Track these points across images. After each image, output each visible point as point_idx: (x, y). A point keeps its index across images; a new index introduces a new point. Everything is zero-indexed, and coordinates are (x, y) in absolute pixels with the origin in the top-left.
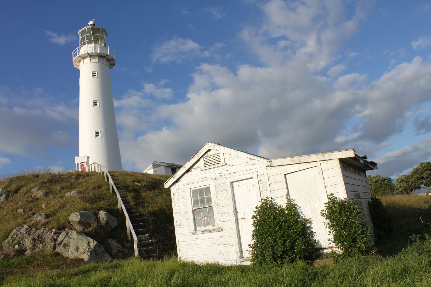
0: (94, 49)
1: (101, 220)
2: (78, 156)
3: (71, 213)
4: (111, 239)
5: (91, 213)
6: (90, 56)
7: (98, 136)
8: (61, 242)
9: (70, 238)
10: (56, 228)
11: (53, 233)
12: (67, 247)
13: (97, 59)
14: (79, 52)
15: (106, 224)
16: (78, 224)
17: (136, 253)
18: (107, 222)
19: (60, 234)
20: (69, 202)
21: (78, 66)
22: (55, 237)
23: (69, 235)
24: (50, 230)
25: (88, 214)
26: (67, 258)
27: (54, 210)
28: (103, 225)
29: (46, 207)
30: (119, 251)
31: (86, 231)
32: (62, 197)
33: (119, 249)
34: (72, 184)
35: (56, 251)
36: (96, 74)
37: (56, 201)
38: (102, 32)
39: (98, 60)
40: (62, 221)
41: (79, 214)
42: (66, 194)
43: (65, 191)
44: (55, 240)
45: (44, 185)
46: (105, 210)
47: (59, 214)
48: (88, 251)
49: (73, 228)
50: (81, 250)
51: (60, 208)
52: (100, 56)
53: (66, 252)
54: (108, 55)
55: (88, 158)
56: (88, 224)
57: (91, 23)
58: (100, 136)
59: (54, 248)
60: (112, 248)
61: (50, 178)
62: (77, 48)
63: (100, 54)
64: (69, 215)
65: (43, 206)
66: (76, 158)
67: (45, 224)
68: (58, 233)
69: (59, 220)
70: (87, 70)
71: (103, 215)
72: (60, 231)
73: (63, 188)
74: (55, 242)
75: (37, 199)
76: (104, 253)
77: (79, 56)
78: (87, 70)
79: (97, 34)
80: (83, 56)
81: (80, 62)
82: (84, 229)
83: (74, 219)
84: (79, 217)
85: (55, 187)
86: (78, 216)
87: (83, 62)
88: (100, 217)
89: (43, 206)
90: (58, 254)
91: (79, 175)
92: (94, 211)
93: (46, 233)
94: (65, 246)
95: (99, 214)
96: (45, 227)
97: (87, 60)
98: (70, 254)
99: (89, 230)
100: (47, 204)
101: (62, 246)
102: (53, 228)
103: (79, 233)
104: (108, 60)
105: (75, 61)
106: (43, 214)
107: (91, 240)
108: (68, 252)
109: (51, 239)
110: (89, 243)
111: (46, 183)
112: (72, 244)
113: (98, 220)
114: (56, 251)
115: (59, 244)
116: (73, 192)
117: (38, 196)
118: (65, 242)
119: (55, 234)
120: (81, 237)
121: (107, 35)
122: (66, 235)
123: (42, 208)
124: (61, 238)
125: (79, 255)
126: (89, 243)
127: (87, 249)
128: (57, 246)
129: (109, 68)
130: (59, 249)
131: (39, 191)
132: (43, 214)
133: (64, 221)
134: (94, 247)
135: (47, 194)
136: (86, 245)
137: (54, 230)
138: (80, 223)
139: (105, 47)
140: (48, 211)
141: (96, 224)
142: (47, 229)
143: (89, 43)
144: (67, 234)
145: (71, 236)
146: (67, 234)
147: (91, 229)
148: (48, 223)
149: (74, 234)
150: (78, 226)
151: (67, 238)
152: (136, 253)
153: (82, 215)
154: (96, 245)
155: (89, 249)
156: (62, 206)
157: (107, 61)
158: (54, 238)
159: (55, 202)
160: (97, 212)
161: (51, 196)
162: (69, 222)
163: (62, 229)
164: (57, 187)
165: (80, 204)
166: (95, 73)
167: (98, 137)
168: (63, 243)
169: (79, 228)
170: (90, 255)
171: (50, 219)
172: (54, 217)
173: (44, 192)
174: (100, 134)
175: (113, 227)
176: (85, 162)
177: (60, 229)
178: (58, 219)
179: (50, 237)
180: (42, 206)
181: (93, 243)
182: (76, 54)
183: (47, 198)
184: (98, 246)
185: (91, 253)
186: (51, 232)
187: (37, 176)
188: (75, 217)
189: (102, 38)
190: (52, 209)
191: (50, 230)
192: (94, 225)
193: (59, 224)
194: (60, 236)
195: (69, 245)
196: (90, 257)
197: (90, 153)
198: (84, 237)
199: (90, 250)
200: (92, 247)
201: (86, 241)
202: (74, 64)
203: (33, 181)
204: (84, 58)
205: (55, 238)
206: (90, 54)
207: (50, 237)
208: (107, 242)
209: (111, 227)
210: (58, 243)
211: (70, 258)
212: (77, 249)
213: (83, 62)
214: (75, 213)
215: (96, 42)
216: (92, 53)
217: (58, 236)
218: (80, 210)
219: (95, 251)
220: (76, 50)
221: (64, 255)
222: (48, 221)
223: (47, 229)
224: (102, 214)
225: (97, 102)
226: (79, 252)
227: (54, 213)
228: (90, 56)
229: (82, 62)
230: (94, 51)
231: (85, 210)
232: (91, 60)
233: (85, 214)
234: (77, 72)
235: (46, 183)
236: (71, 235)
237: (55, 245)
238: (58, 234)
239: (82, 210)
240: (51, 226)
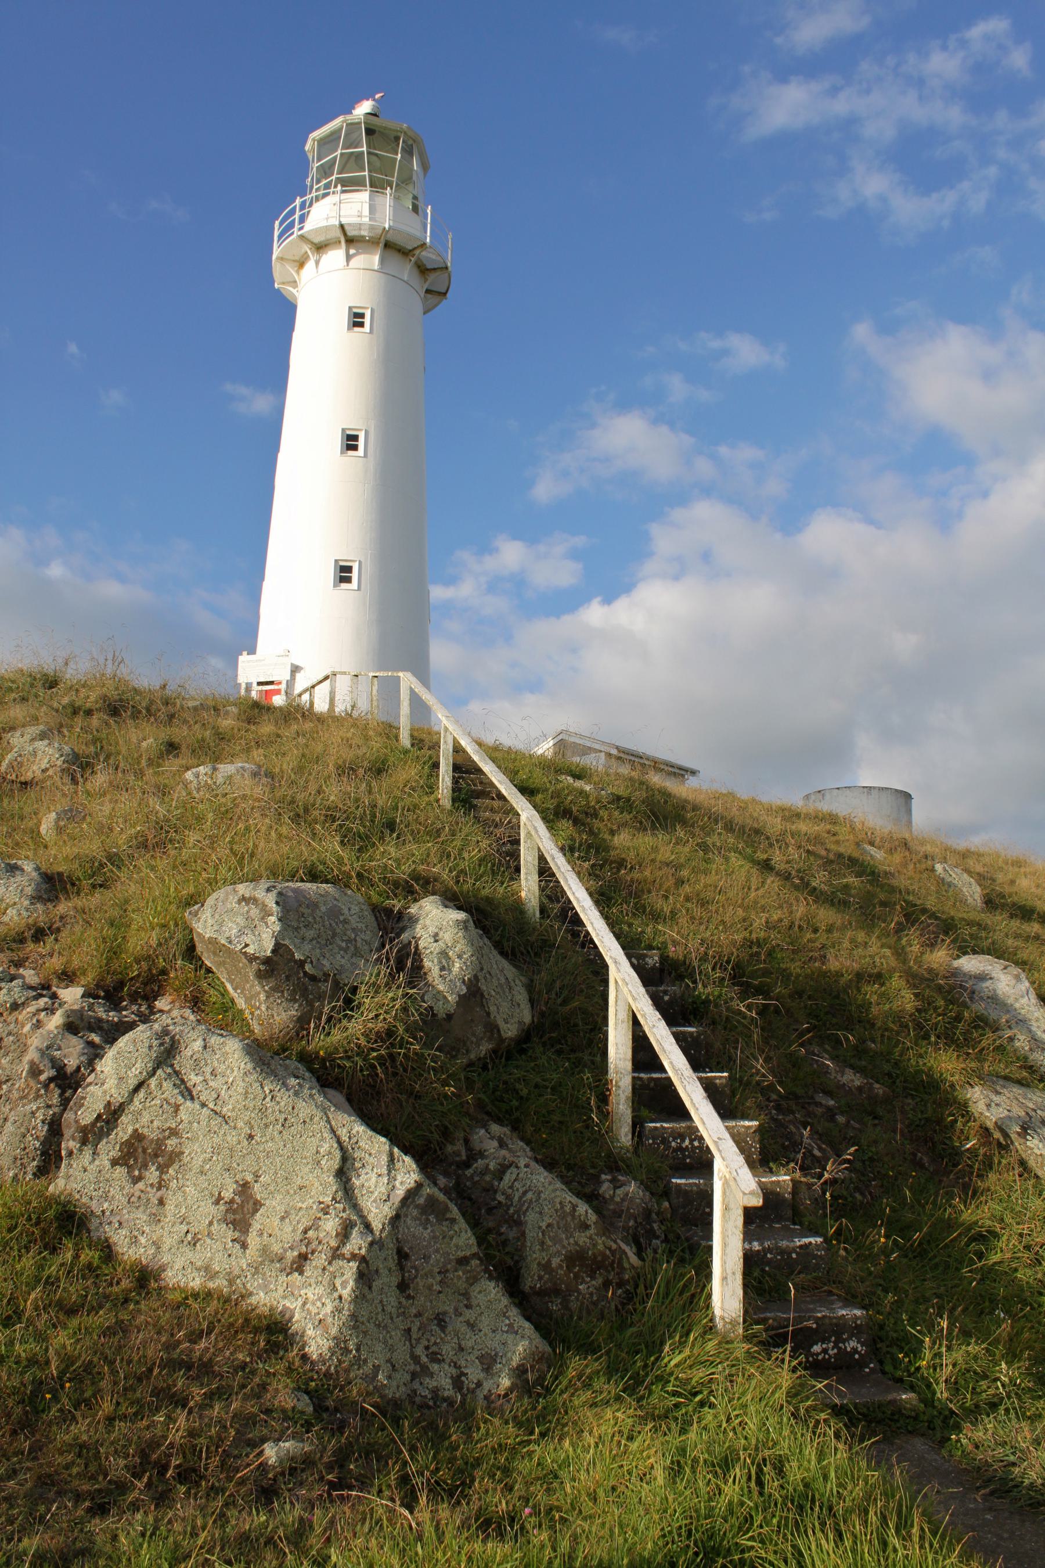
0: (366, 211)
1: (431, 964)
2: (252, 651)
3: (213, 884)
4: (495, 1128)
5: (353, 906)
6: (351, 240)
7: (348, 580)
8: (112, 1115)
9: (188, 1093)
10: (90, 977)
11: (56, 1021)
12: (152, 1174)
13: (376, 258)
14: (302, 219)
15: (463, 1000)
16: (260, 975)
17: (726, 1295)
18: (473, 994)
19: (113, 1033)
20: (200, 819)
21: (294, 283)
22: (72, 1054)
23: (183, 1061)
24: (44, 988)
25: (335, 913)
26: (145, 1278)
27: (101, 856)
28: (441, 1010)
29: (60, 830)
30: (577, 1258)
31: (319, 1042)
32: (163, 791)
33: (582, 1239)
34: (221, 737)
35: (59, 1185)
36: (367, 321)
37: (127, 803)
38: (408, 152)
39: (382, 261)
40: (142, 938)
41: (270, 901)
42: (189, 775)
43: (181, 761)
44: (67, 1082)
45: (79, 721)
46: (452, 899)
47: (127, 886)
48: (336, 1254)
49: (213, 995)
50: (275, 1226)
51: (144, 845)
52: (392, 247)
53: (141, 1216)
54: (423, 245)
55: (295, 669)
56: (337, 986)
57: (365, 107)
58: (354, 584)
59: (50, 1158)
60: (518, 1224)
61: (114, 694)
62: (298, 201)
63: (390, 237)
64: (194, 900)
65: (47, 825)
66: (244, 659)
67: (21, 940)
68: (96, 1026)
69: (119, 924)
70: (330, 303)
71: (447, 936)
72: (116, 1006)
73: (172, 747)
74: (65, 1103)
75: (25, 784)
76: (473, 1280)
77: (302, 237)
78: (330, 303)
79: (384, 153)
80: (317, 240)
81: (301, 264)
82: (302, 1022)
83: (231, 929)
84: (273, 924)
85: (134, 735)
86: (266, 913)
87: (317, 263)
88: (425, 942)
89: (47, 825)
90: (70, 1221)
91: (256, 710)
92: (375, 898)
93: (15, 1007)
94: (137, 1155)
95: (413, 920)
96: (19, 964)
97: (336, 256)
98: (172, 1237)
99: (337, 1036)
100: (71, 815)
101: (109, 1148)
102: (68, 977)
103: (269, 1055)
104: (423, 270)
105: (281, 259)
106: (28, 867)
107: (373, 1147)
108: (156, 1219)
109: (35, 1071)
110: (344, 1173)
111: (89, 713)
112: (196, 1151)
113: (407, 964)
114: (59, 1185)
115: (93, 1134)
116: (226, 769)
117: (32, 771)
118: (144, 1118)
119: (71, 1027)
120: (285, 1098)
121: (425, 166)
122: (158, 1064)
123: (35, 833)
124: (111, 1083)
125: (256, 1269)
126: (344, 1173)
127: (331, 1225)
128: (69, 1143)
129: (419, 308)
130: (86, 1177)
131: (41, 745)
132: (28, 867)
133: (154, 937)
134: (396, 1220)
135: (79, 766)
136: (322, 1185)
137: (71, 995)
138: (275, 967)
139: (415, 209)
140: (61, 857)
141: (393, 998)
142: (30, 975)
143: (350, 185)
144: (167, 1052)
145: (193, 1079)
146: (167, 1052)
147: (355, 1028)
148: (39, 934)
149: (224, 1066)
150: (259, 991)
151: (163, 1088)
152: (726, 1295)
153: (293, 912)
154: (411, 1195)
155: (344, 1235)
156: (158, 839)
157: (417, 269)
158: (60, 1068)
159: (116, 810)
160: (397, 905)
161: (100, 779)
162: (190, 952)
163: (134, 998)
164: (143, 738)
165: (276, 841)
166: (362, 316)
167: (344, 586)
168: (125, 1129)
169: (266, 1010)
170: (359, 1298)
171: (63, 907)
172: (96, 899)
173: (67, 749)
174: (355, 575)
175: (510, 1031)
176: (280, 683)
177: (124, 993)
178: (116, 913)
179: (36, 1042)
180: (39, 824)
181: (386, 1179)
182: (291, 225)
183: (74, 781)
184: (432, 1207)
185: (365, 1277)
186: (51, 1010)
187: (52, 683)
188: (239, 922)
189: (406, 180)
190: (93, 848)
191: (44, 988)
192: (377, 1009)
193: (115, 952)
194: (107, 1065)
195: (175, 1157)
196: (355, 1321)
197: (304, 633)
198: (305, 1109)
199: (357, 1243)
200: (378, 1214)
201: (328, 1145)
202: (279, 272)
203: (24, 699)
204: (320, 248)
205: (72, 1063)
206: (351, 233)
207: (32, 1055)
208: (474, 1155)
209: (492, 1028)
210: (86, 1117)
211: (172, 1277)
212: (240, 1211)
213: (317, 263)
214: (243, 889)
215: (377, 186)
216: (360, 226)
217: (95, 1053)
218: (274, 873)
219: (402, 1255)
220: (293, 212)
221: (120, 1239)
222: (42, 921)
223: (30, 975)
224: (437, 927)
225: (349, 569)
226: (253, 1240)
227: (101, 873)
228: (351, 240)
229: (310, 265)
230: (366, 220)
231: (314, 876)
232: (349, 257)
233: (314, 906)
234: (284, 313)
235: (89, 713)
236: (197, 1066)
237: (55, 1128)
238: (97, 1032)
239: (292, 876)
240: (56, 963)
